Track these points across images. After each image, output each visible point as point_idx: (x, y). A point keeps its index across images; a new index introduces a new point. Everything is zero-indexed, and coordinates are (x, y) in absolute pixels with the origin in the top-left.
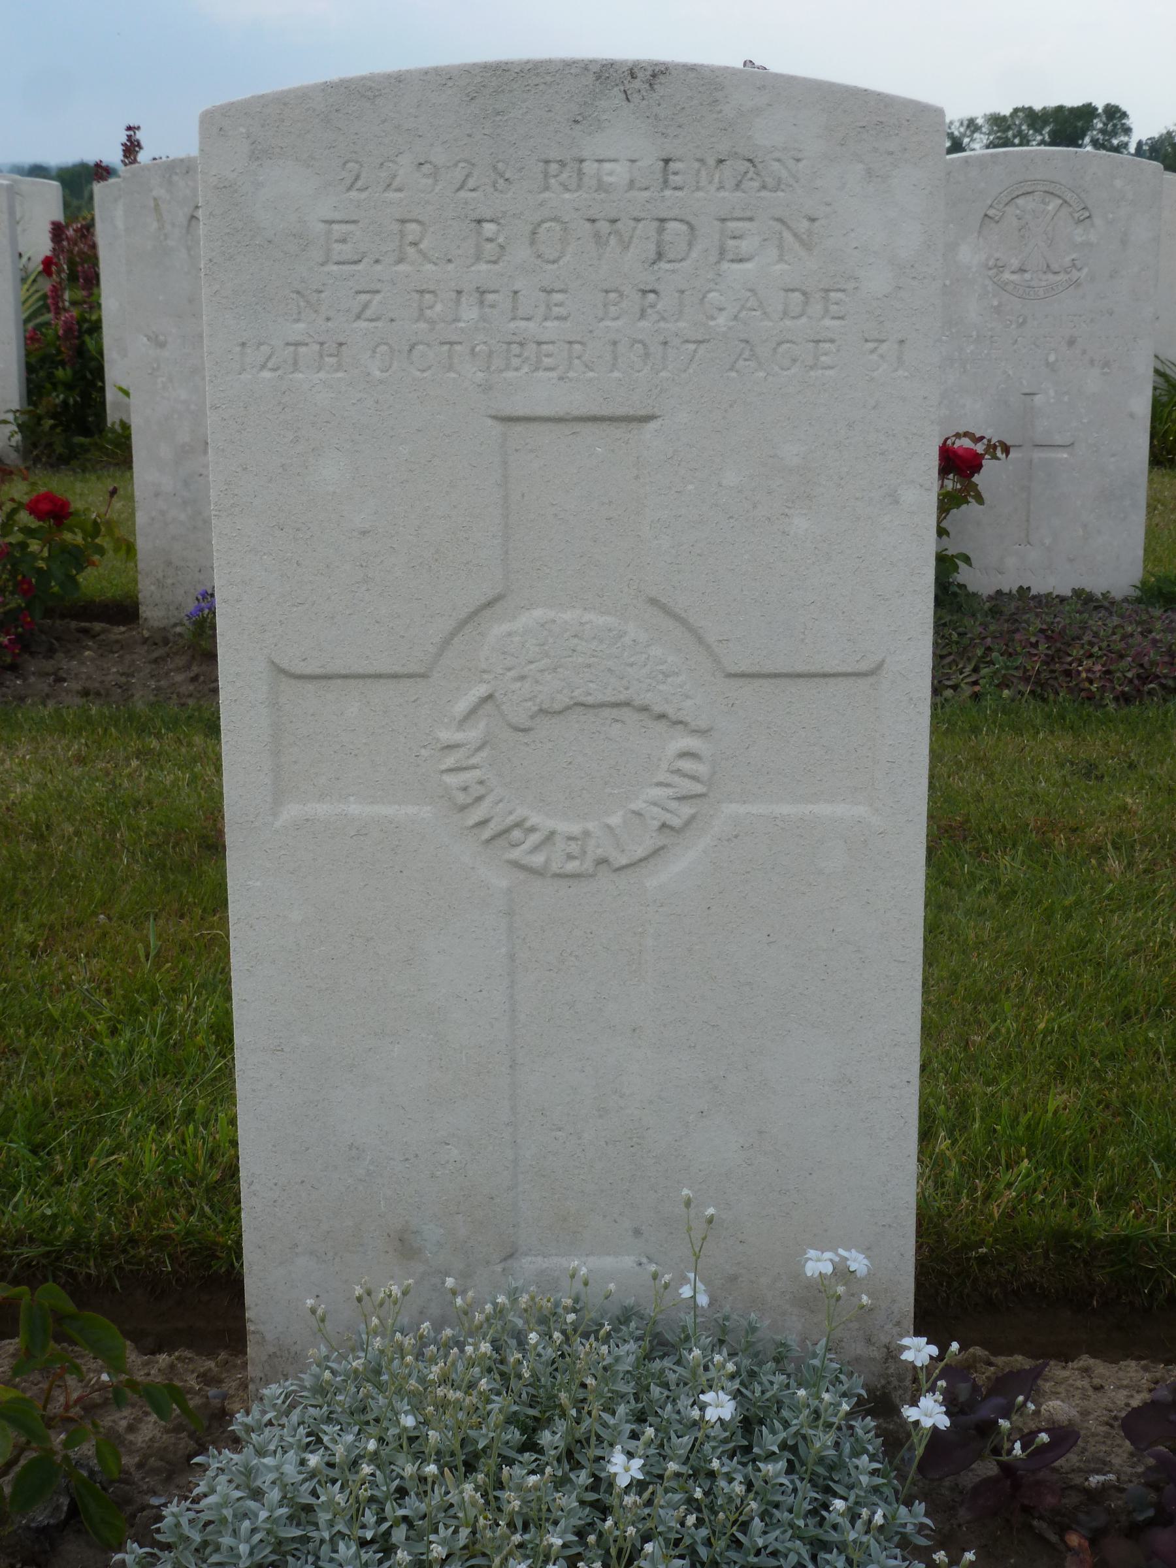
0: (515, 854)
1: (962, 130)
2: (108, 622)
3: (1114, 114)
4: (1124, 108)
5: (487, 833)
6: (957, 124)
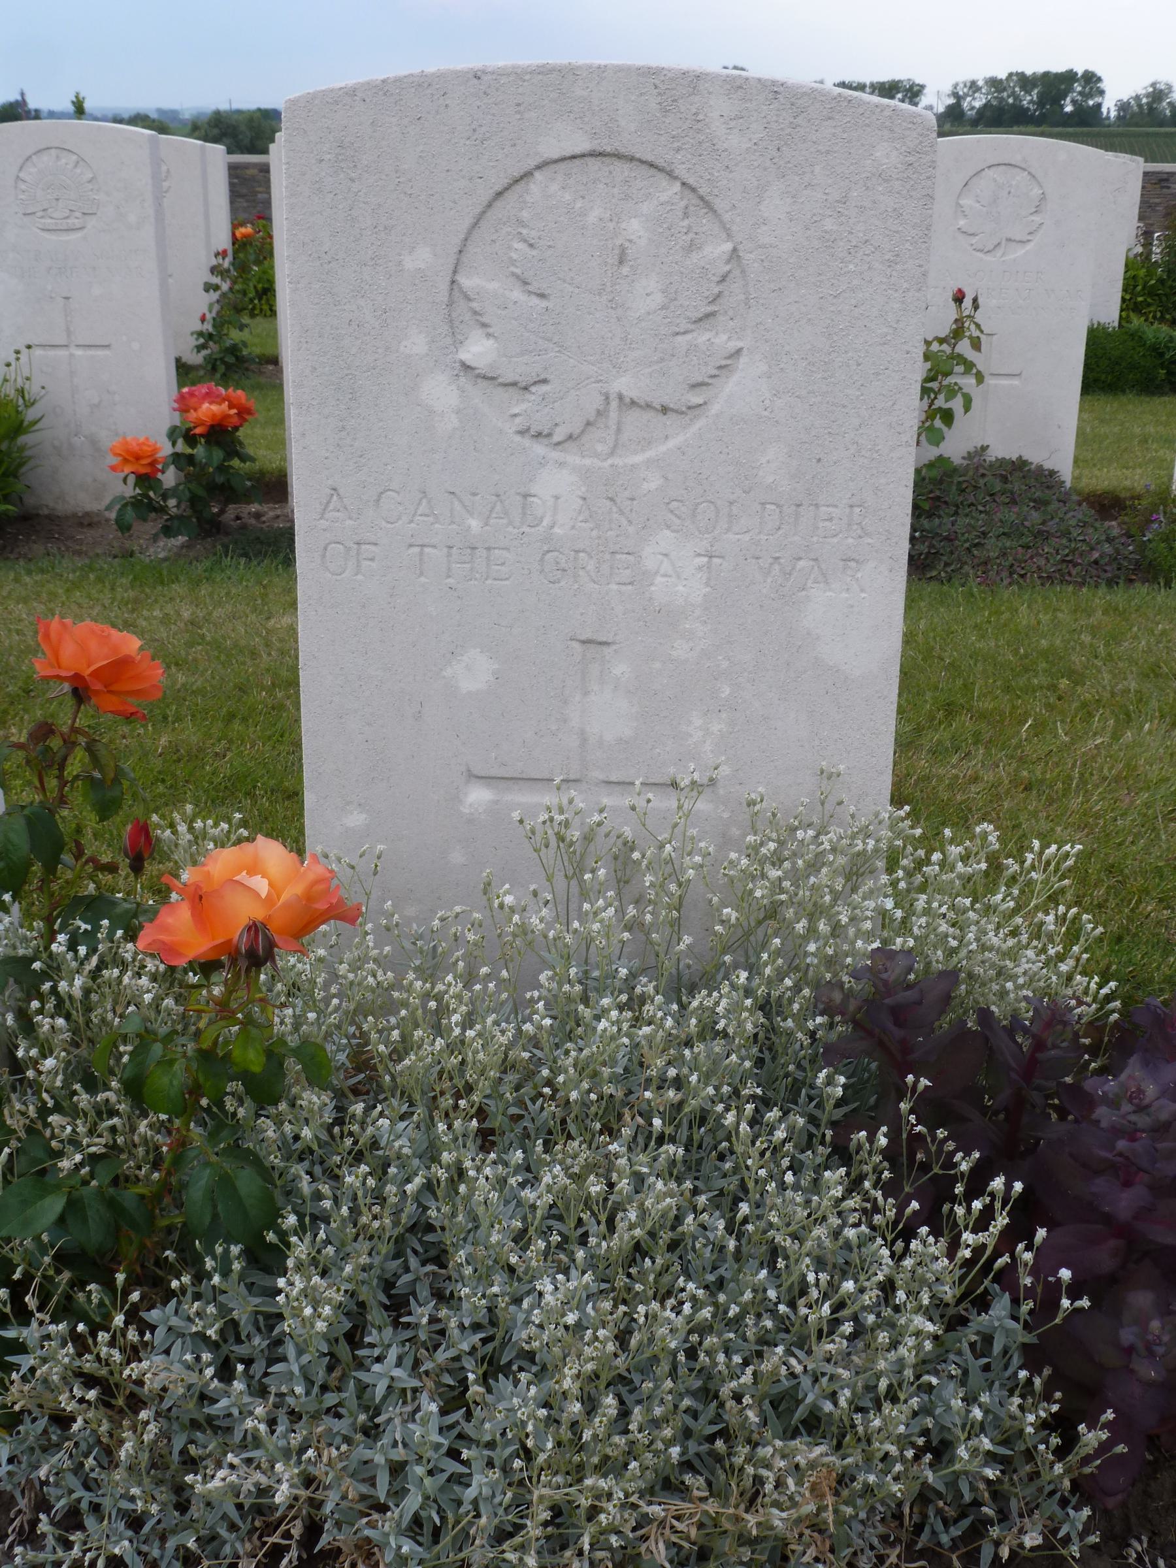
4: (1099, 73)
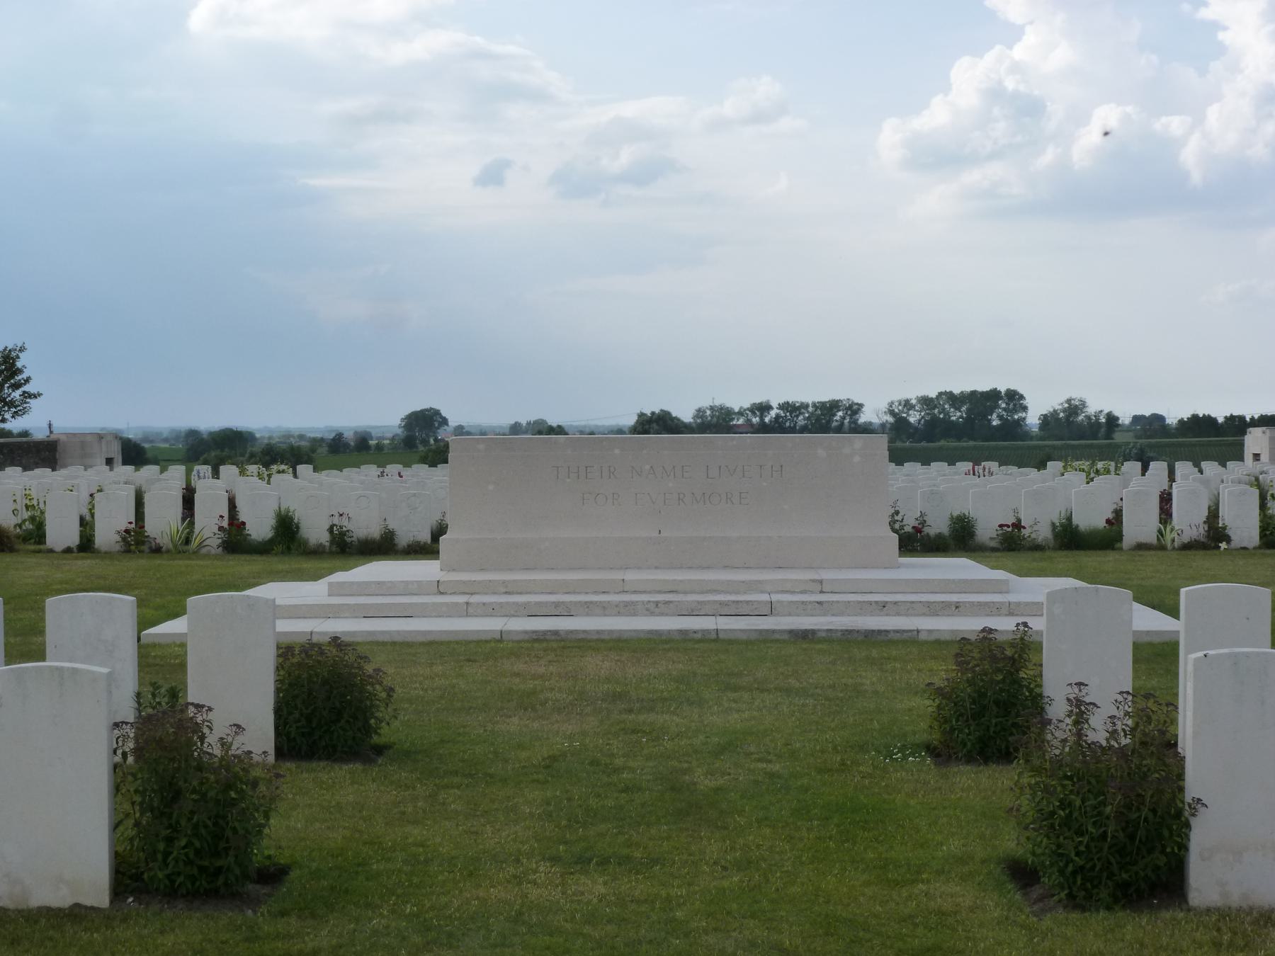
6: (897, 404)
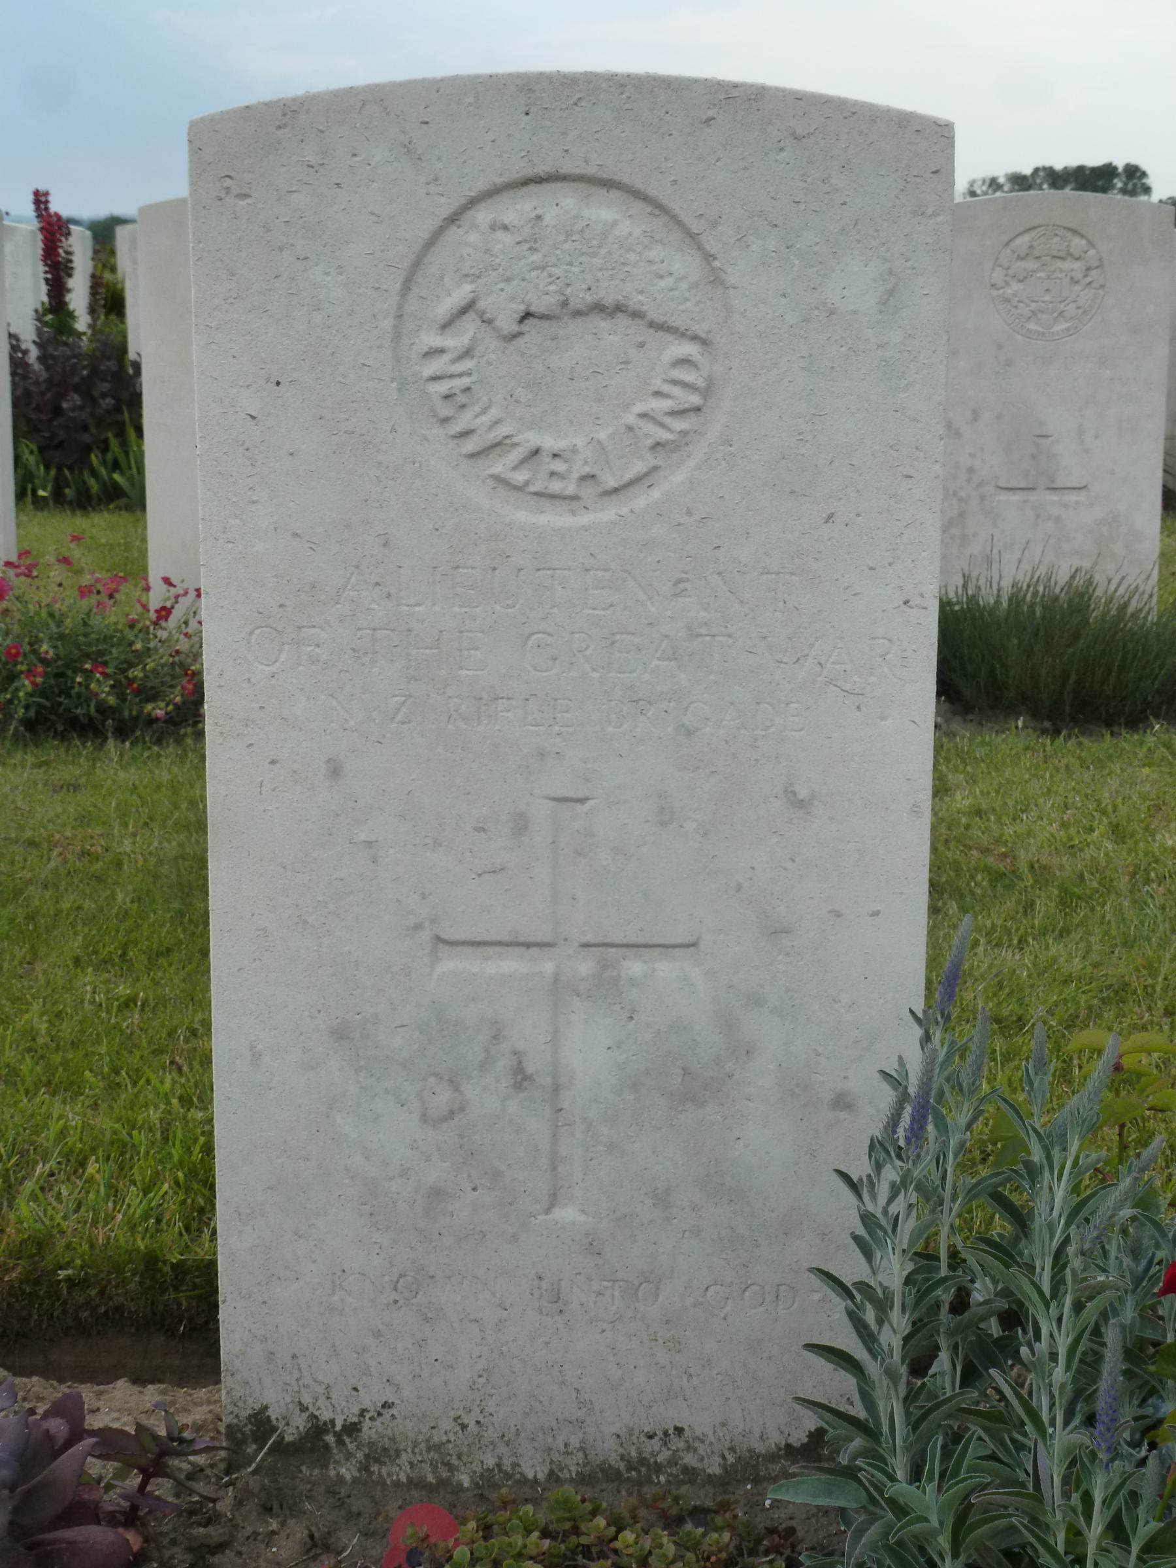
0: (497, 469)
1: (984, 188)
2: (110, 1429)
3: (1134, 173)
5: (470, 446)
6: (980, 183)
